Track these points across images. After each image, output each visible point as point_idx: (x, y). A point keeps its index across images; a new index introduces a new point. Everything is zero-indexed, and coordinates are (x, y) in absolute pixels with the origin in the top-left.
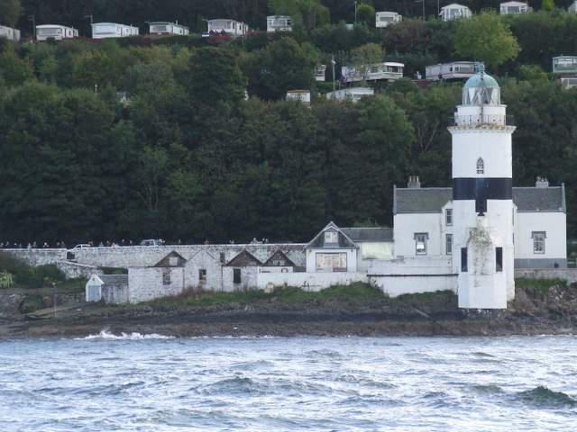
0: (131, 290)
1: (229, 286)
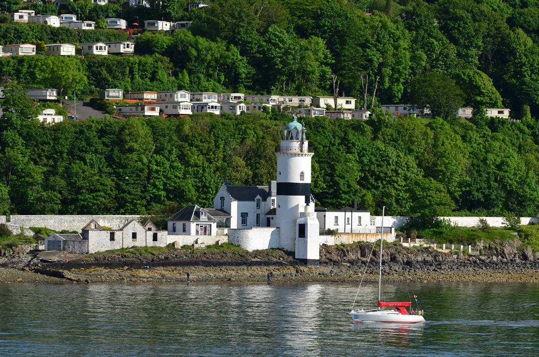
0: (90, 244)
1: (151, 243)
